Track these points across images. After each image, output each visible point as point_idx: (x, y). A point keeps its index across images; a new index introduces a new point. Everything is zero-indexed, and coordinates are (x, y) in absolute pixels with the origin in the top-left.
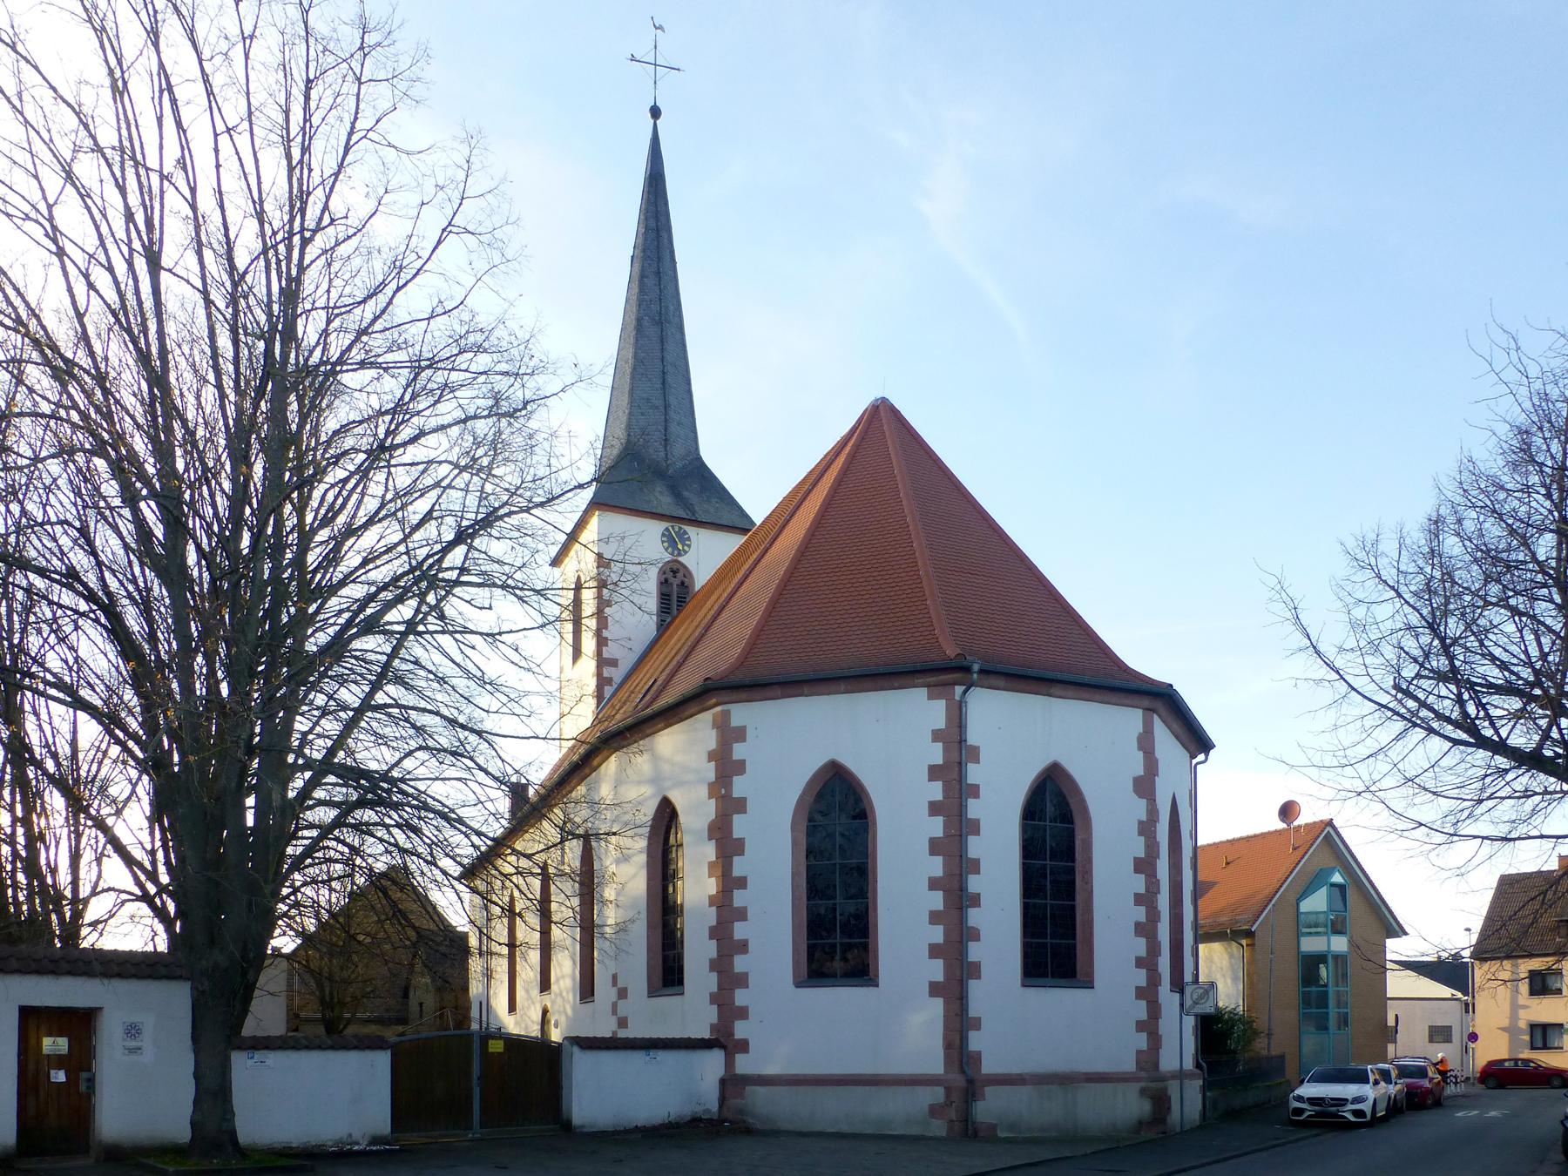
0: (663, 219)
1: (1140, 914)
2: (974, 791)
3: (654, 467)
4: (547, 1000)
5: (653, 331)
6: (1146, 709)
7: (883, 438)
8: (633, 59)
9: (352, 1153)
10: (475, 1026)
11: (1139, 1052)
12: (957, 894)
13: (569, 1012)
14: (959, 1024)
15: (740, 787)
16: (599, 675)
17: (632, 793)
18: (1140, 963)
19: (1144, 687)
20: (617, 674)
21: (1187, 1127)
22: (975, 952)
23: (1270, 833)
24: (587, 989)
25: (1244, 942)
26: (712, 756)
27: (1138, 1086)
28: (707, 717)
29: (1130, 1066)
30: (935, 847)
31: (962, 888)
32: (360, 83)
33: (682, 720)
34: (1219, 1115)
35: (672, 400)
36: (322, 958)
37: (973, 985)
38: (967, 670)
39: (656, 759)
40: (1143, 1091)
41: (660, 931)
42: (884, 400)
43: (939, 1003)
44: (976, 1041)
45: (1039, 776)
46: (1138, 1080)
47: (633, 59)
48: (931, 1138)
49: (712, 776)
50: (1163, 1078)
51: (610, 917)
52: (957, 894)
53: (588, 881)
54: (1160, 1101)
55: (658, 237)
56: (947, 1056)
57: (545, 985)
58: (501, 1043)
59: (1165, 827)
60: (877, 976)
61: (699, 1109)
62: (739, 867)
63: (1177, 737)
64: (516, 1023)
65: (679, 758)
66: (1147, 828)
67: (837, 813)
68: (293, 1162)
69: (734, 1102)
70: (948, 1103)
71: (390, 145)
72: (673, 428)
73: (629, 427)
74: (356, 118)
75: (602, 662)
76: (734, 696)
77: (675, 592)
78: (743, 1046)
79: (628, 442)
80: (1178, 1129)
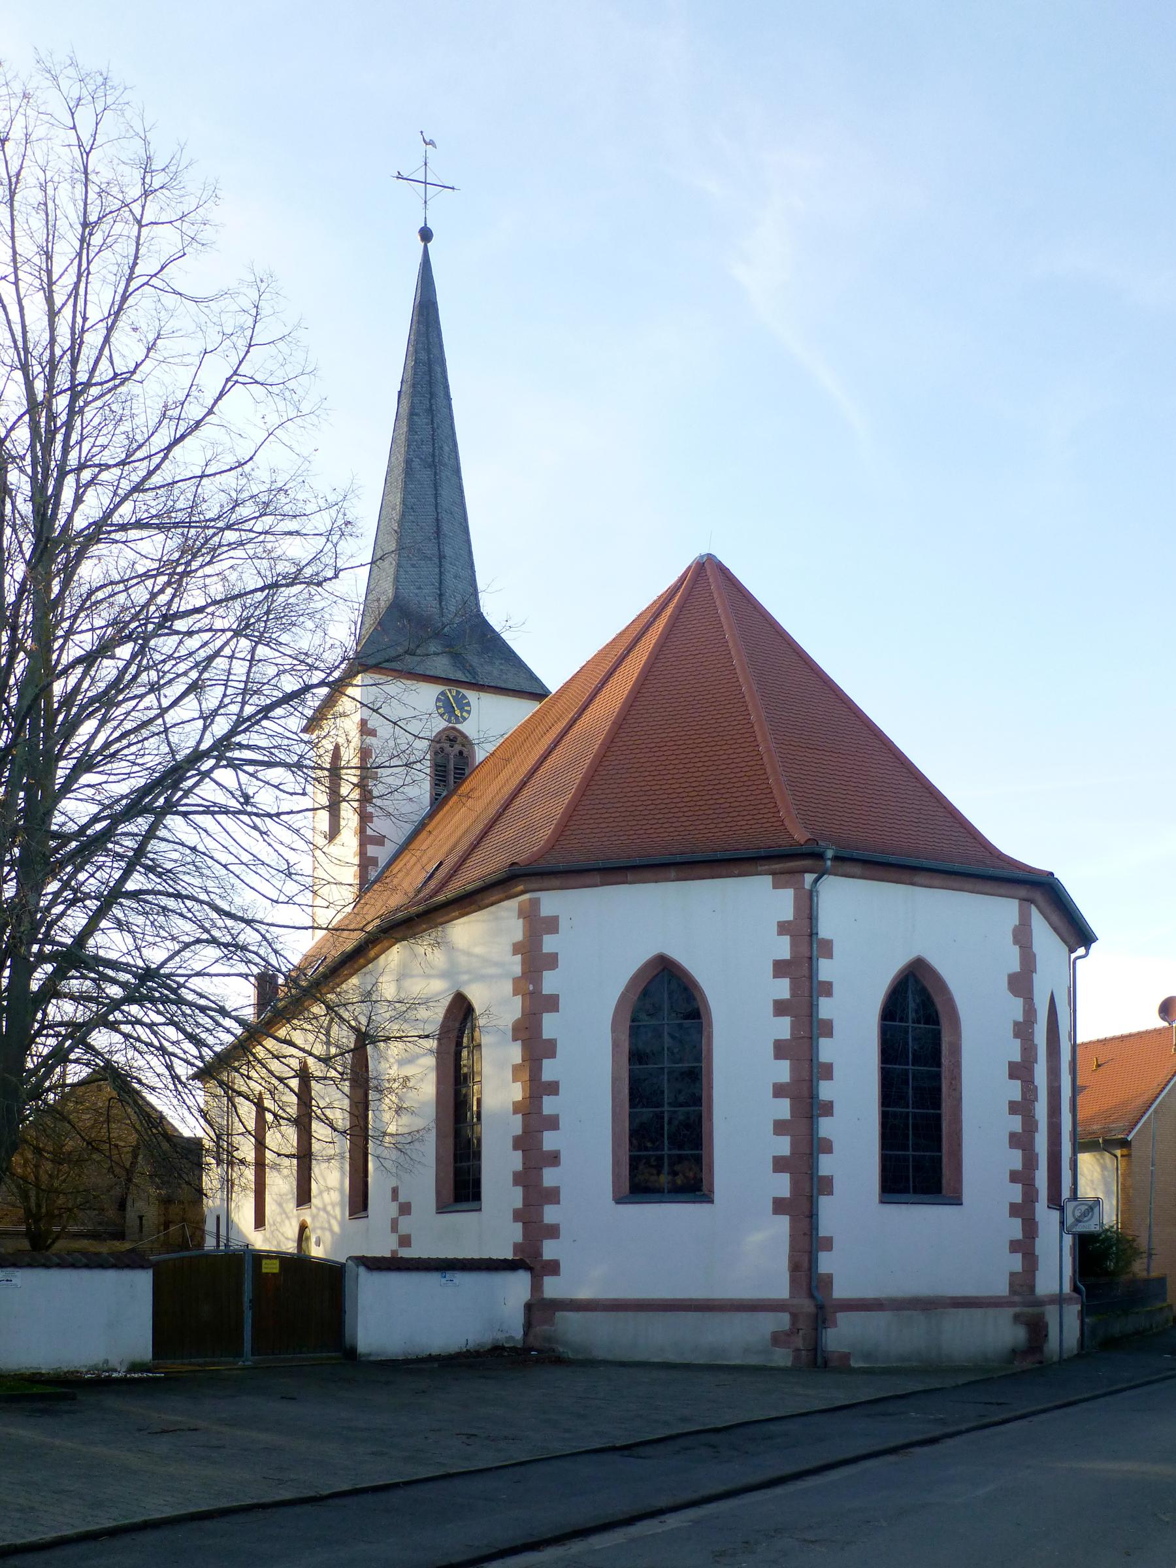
0: (435, 351)
1: (1016, 1123)
2: (827, 989)
3: (429, 623)
4: (307, 1215)
5: (425, 475)
6: (1022, 900)
7: (709, 601)
8: (399, 177)
9: (109, 1381)
10: (210, 1243)
11: (1012, 1274)
12: (806, 1102)
13: (336, 1228)
14: (807, 1243)
15: (550, 983)
16: (362, 853)
17: (417, 987)
18: (1014, 1177)
19: (1020, 874)
20: (382, 854)
21: (1065, 1356)
22: (826, 1165)
23: (1147, 1032)
24: (359, 1202)
25: (1118, 1152)
26: (517, 949)
27: (1011, 1311)
28: (513, 904)
29: (1001, 1288)
30: (781, 1050)
31: (813, 1095)
32: (141, 226)
33: (480, 908)
34: (1099, 1344)
35: (448, 551)
36: (25, 1166)
37: (824, 1201)
38: (820, 856)
39: (451, 949)
40: (1017, 1318)
41: (450, 1141)
42: (710, 557)
43: (784, 1222)
44: (826, 1263)
45: (902, 972)
46: (1011, 1304)
47: (399, 177)
48: (772, 1369)
49: (517, 970)
50: (1040, 1303)
51: (387, 1119)
52: (806, 1102)
53: (362, 1085)
54: (1036, 1329)
55: (430, 371)
56: (793, 1281)
57: (304, 1197)
58: (276, 1263)
59: (1043, 1028)
60: (712, 1191)
61: (500, 1337)
62: (550, 1070)
63: (1055, 929)
64: (266, 1240)
65: (478, 950)
66: (1023, 1030)
67: (666, 1015)
68: (50, 1390)
69: (540, 1329)
70: (794, 1330)
71: (175, 292)
72: (449, 577)
73: (396, 579)
74: (135, 264)
75: (365, 840)
76: (546, 882)
77: (451, 765)
78: (553, 1268)
79: (396, 596)
80: (1056, 1358)
